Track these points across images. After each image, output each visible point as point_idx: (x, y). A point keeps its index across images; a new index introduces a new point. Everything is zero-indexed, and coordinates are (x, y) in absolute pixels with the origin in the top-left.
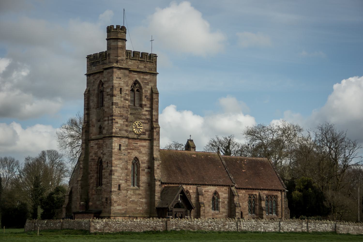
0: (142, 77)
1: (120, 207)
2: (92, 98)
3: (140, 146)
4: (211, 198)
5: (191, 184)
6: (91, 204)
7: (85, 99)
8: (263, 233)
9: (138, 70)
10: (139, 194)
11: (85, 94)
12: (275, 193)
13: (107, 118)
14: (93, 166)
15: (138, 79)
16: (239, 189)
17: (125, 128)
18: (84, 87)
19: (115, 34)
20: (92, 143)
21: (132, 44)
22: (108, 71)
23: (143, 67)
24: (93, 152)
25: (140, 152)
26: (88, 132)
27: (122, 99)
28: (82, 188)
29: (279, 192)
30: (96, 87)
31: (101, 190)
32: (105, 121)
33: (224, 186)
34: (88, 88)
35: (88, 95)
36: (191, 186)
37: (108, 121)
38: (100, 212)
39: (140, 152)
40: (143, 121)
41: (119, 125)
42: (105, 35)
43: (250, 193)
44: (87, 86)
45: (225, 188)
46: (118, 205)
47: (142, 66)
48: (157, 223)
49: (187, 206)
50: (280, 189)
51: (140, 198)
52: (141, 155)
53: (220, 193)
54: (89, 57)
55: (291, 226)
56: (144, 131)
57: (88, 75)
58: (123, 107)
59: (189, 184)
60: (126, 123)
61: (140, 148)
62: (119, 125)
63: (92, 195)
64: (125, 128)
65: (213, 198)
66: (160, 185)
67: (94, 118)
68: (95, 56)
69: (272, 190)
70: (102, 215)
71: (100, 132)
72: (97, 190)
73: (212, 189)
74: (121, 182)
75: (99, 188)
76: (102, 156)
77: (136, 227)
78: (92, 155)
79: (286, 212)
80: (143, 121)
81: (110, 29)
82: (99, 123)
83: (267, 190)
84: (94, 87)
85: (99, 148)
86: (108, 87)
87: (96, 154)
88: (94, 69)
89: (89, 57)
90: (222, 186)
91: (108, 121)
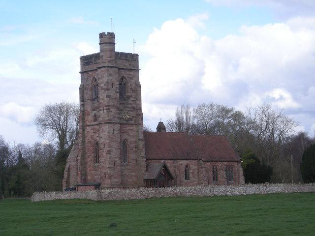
0: (128, 73)
1: (116, 180)
2: (86, 91)
3: (129, 130)
4: (184, 171)
5: (169, 159)
6: (89, 178)
7: (80, 92)
8: (288, 193)
9: (124, 68)
10: (129, 169)
11: (80, 88)
12: (233, 164)
13: (102, 108)
14: (90, 148)
15: (125, 75)
16: (205, 161)
17: (117, 116)
18: (78, 82)
19: (107, 40)
20: (88, 129)
21: (121, 47)
22: (101, 69)
23: (128, 65)
24: (89, 135)
25: (129, 135)
26: (84, 119)
27: (114, 92)
28: (81, 165)
29: (236, 163)
30: (89, 82)
31: (98, 166)
32: (101, 110)
33: (194, 160)
34: (135, 79)
35: (82, 89)
36: (169, 161)
37: (103, 110)
38: (100, 185)
39: (129, 135)
40: (130, 109)
41: (112, 113)
42: (98, 41)
43: (214, 164)
44: (81, 82)
45: (195, 161)
46: (115, 178)
47: (127, 64)
48: (150, 192)
49: (166, 178)
50: (237, 160)
51: (131, 172)
52: (129, 137)
53: (191, 166)
54: (137, 55)
55: (253, 189)
56: (131, 117)
57: (82, 73)
58: (115, 99)
59: (167, 159)
60: (118, 111)
61: (129, 131)
62: (112, 113)
63: (90, 170)
64: (117, 116)
65: (186, 170)
66: (145, 161)
67: (89, 108)
68: (85, 57)
69: (230, 161)
70: (101, 186)
71: (95, 120)
72: (95, 166)
73: (185, 162)
74: (116, 159)
75: (96, 165)
76: (98, 139)
77: (132, 195)
78: (88, 139)
79: (242, 179)
80: (130, 109)
81: (102, 35)
82: (94, 112)
83: (227, 161)
84: (88, 83)
85: (95, 132)
86: (102, 83)
87: (92, 137)
88: (88, 68)
89: (137, 55)
90: (193, 159)
91: (103, 110)
